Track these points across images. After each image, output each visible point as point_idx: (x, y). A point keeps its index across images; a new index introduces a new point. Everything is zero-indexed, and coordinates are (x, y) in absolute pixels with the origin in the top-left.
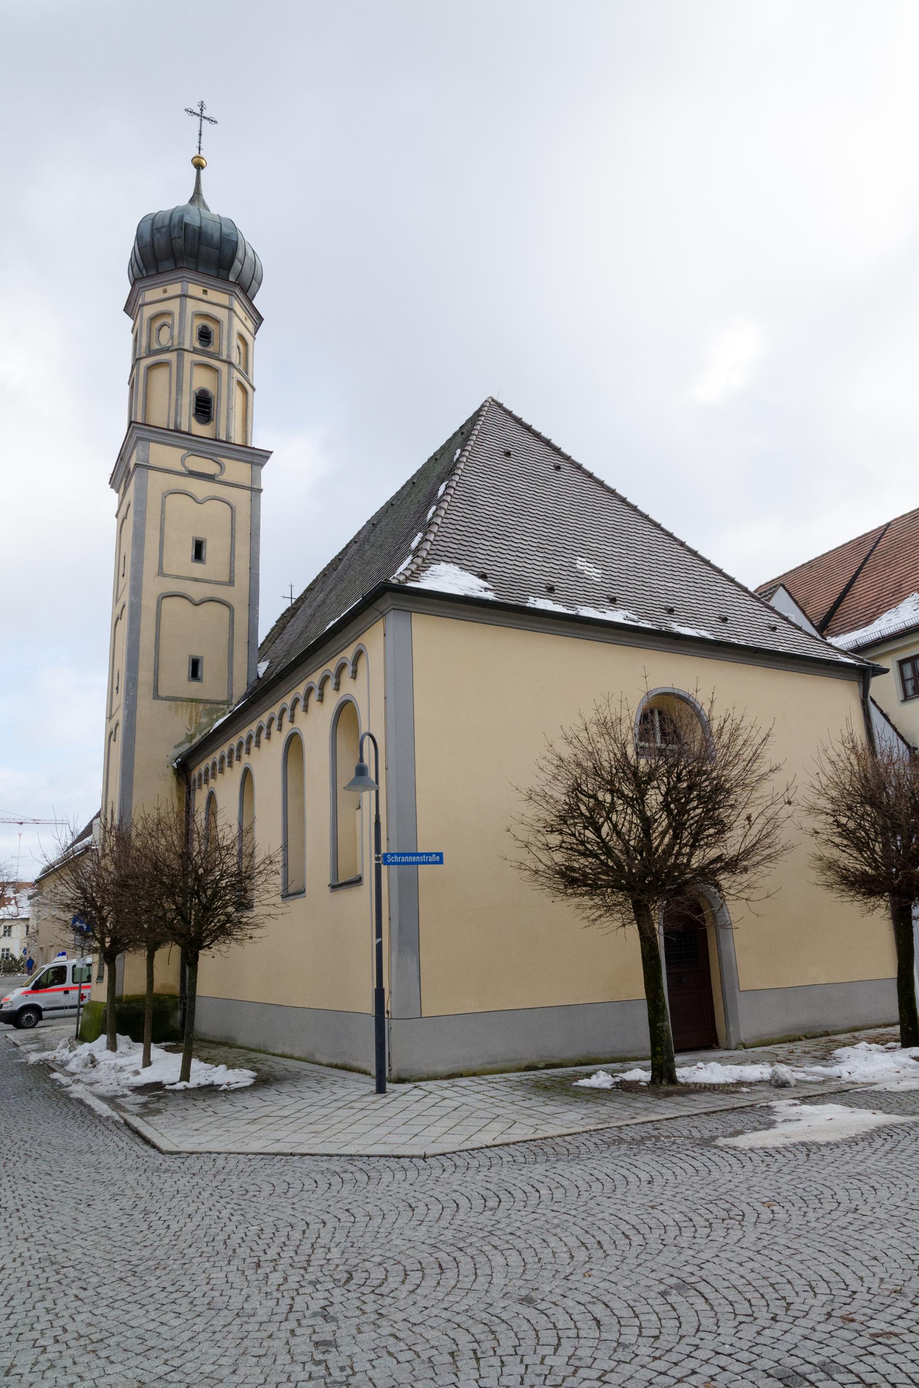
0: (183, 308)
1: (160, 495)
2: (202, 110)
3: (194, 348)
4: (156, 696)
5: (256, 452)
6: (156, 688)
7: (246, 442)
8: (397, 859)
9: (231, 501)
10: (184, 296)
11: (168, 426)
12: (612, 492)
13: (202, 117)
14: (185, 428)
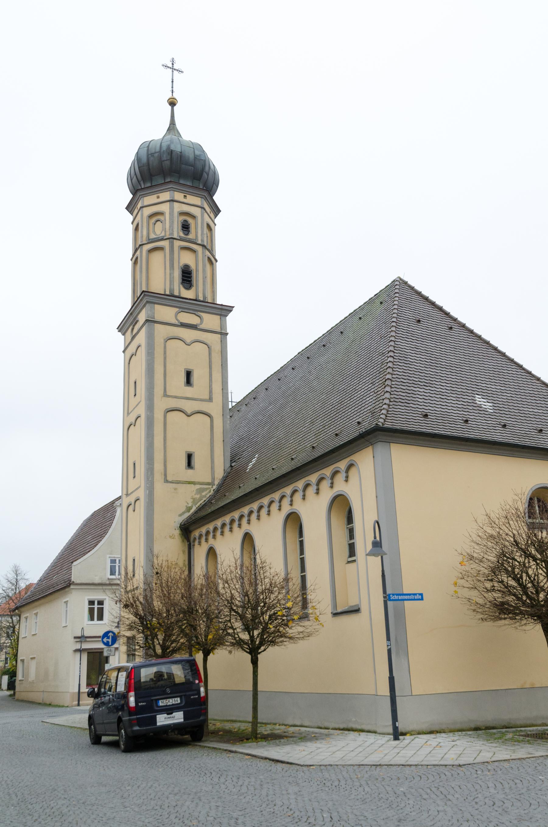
0: (172, 209)
1: (163, 341)
2: (173, 64)
3: (180, 237)
4: (166, 481)
5: (223, 307)
6: (165, 475)
7: (214, 299)
8: (396, 597)
9: (208, 342)
10: (172, 201)
11: (165, 291)
12: (488, 343)
13: (173, 69)
14: (176, 293)
